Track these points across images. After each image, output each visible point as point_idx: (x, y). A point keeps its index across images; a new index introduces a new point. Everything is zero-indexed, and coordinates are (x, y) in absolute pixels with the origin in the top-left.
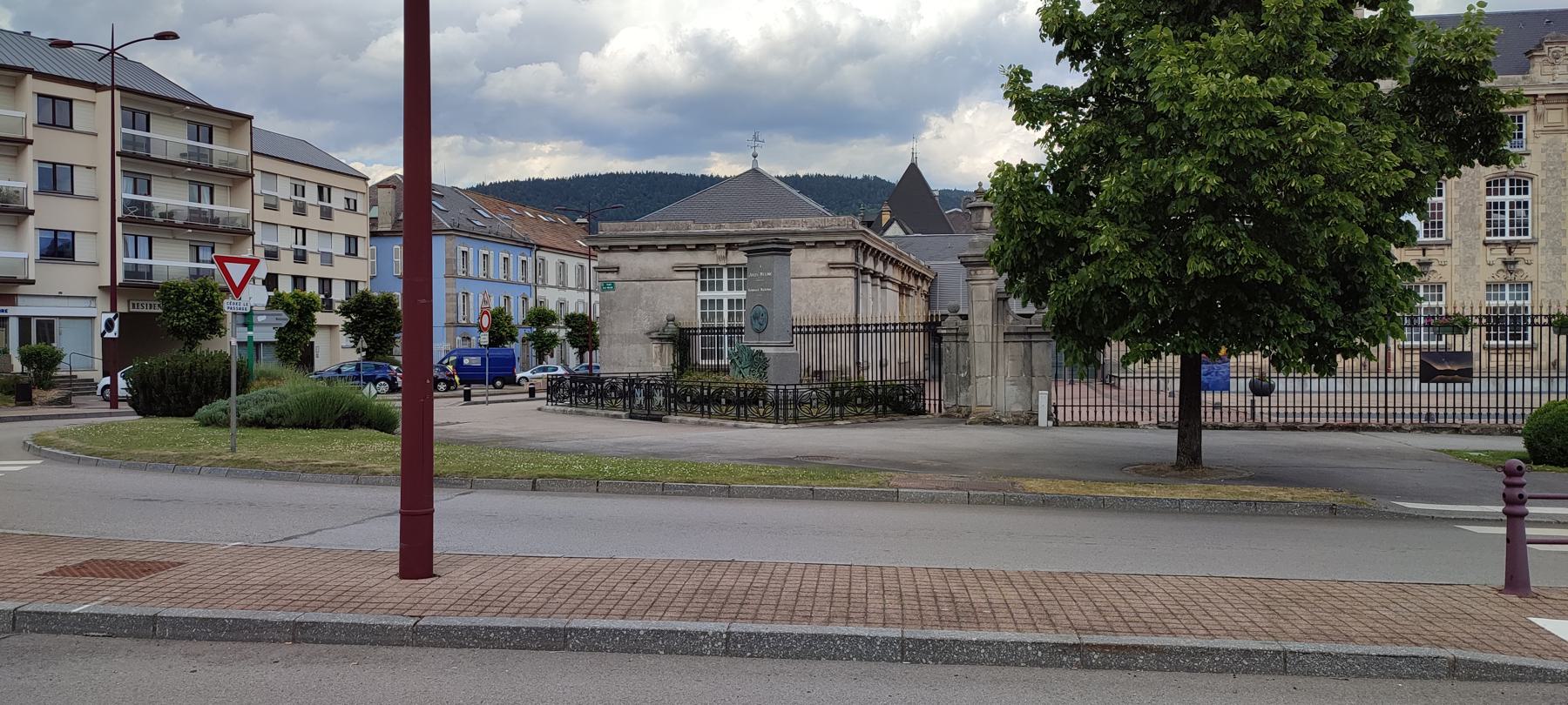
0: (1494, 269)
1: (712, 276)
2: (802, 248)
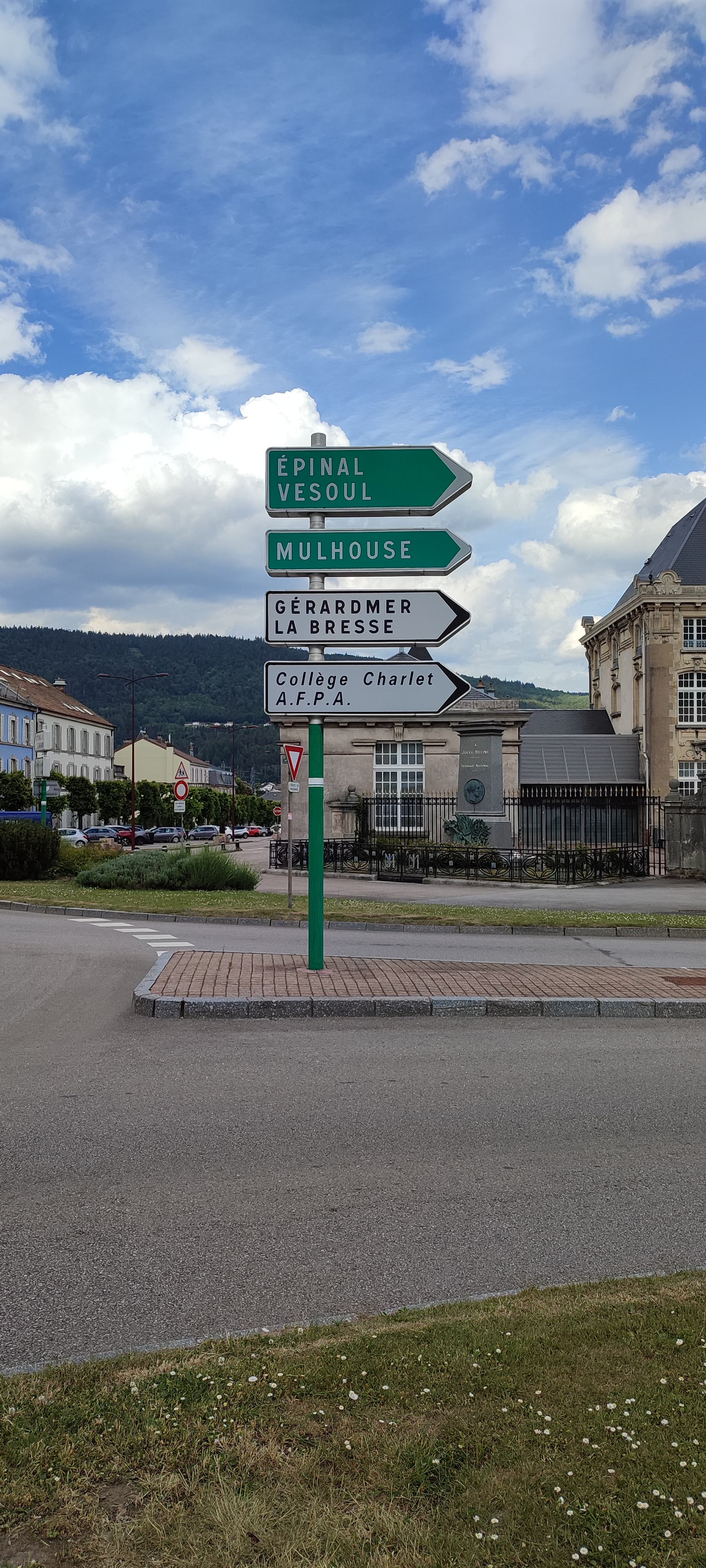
0: (684, 749)
1: (386, 751)
2: (419, 727)
